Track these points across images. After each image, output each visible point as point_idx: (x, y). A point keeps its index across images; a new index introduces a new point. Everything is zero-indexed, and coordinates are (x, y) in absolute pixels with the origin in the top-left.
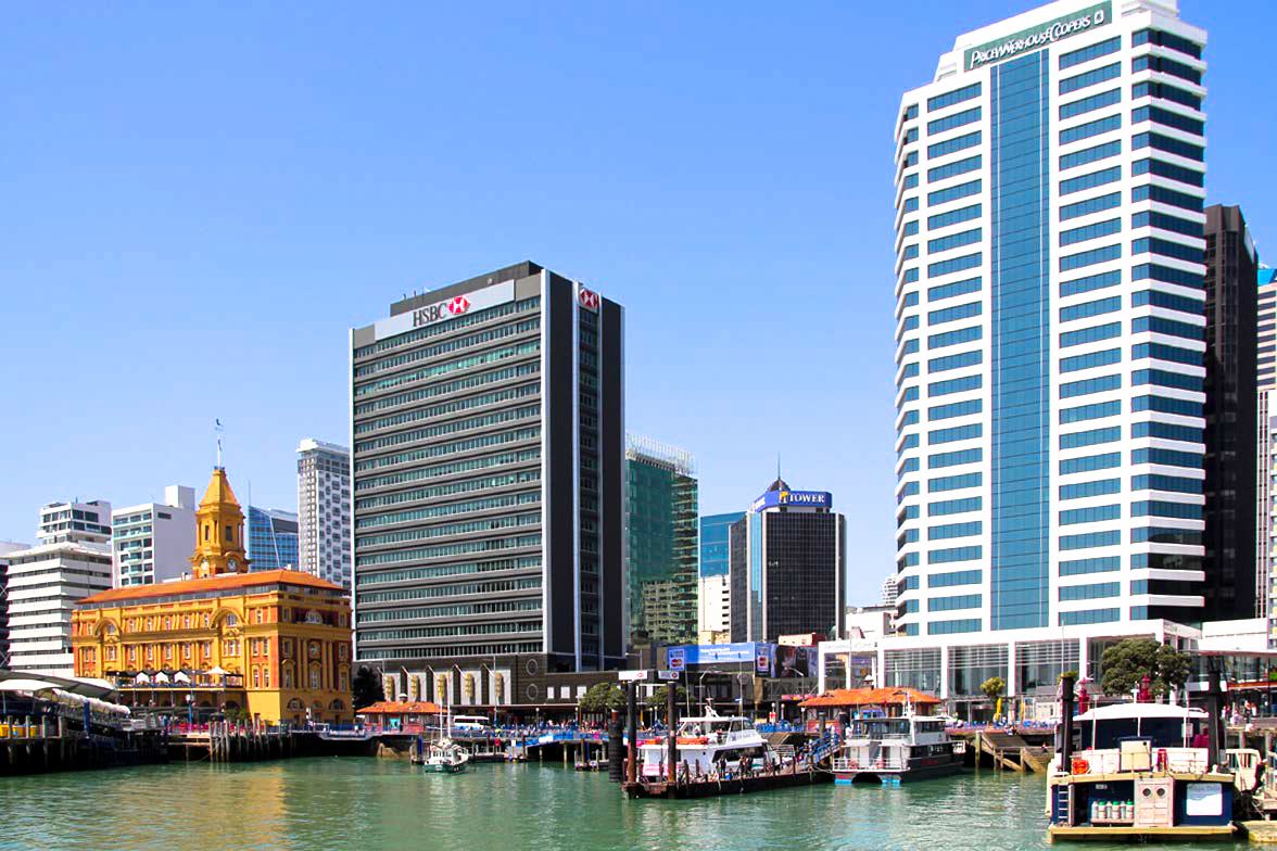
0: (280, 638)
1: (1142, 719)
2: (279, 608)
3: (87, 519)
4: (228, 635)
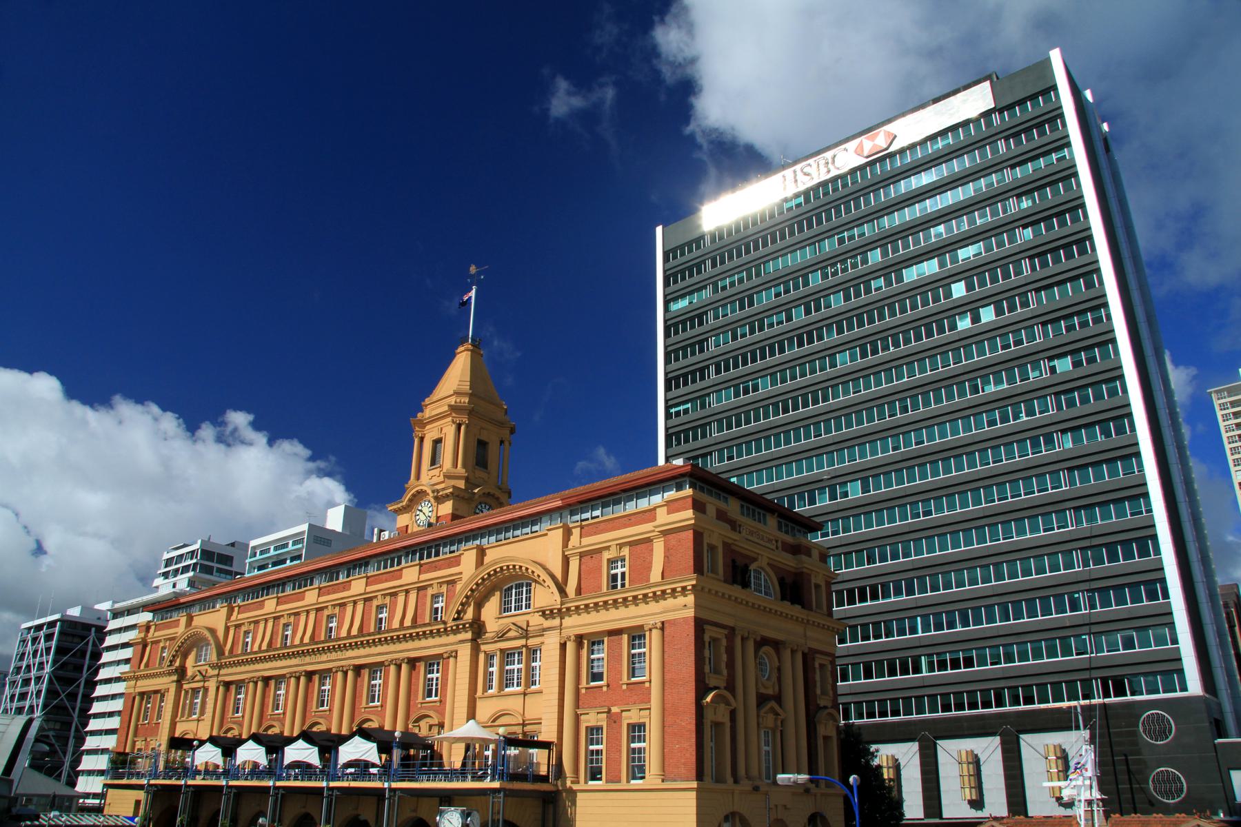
0: (700, 624)
1: (1179, 648)
2: (698, 537)
3: (218, 562)
4: (502, 636)
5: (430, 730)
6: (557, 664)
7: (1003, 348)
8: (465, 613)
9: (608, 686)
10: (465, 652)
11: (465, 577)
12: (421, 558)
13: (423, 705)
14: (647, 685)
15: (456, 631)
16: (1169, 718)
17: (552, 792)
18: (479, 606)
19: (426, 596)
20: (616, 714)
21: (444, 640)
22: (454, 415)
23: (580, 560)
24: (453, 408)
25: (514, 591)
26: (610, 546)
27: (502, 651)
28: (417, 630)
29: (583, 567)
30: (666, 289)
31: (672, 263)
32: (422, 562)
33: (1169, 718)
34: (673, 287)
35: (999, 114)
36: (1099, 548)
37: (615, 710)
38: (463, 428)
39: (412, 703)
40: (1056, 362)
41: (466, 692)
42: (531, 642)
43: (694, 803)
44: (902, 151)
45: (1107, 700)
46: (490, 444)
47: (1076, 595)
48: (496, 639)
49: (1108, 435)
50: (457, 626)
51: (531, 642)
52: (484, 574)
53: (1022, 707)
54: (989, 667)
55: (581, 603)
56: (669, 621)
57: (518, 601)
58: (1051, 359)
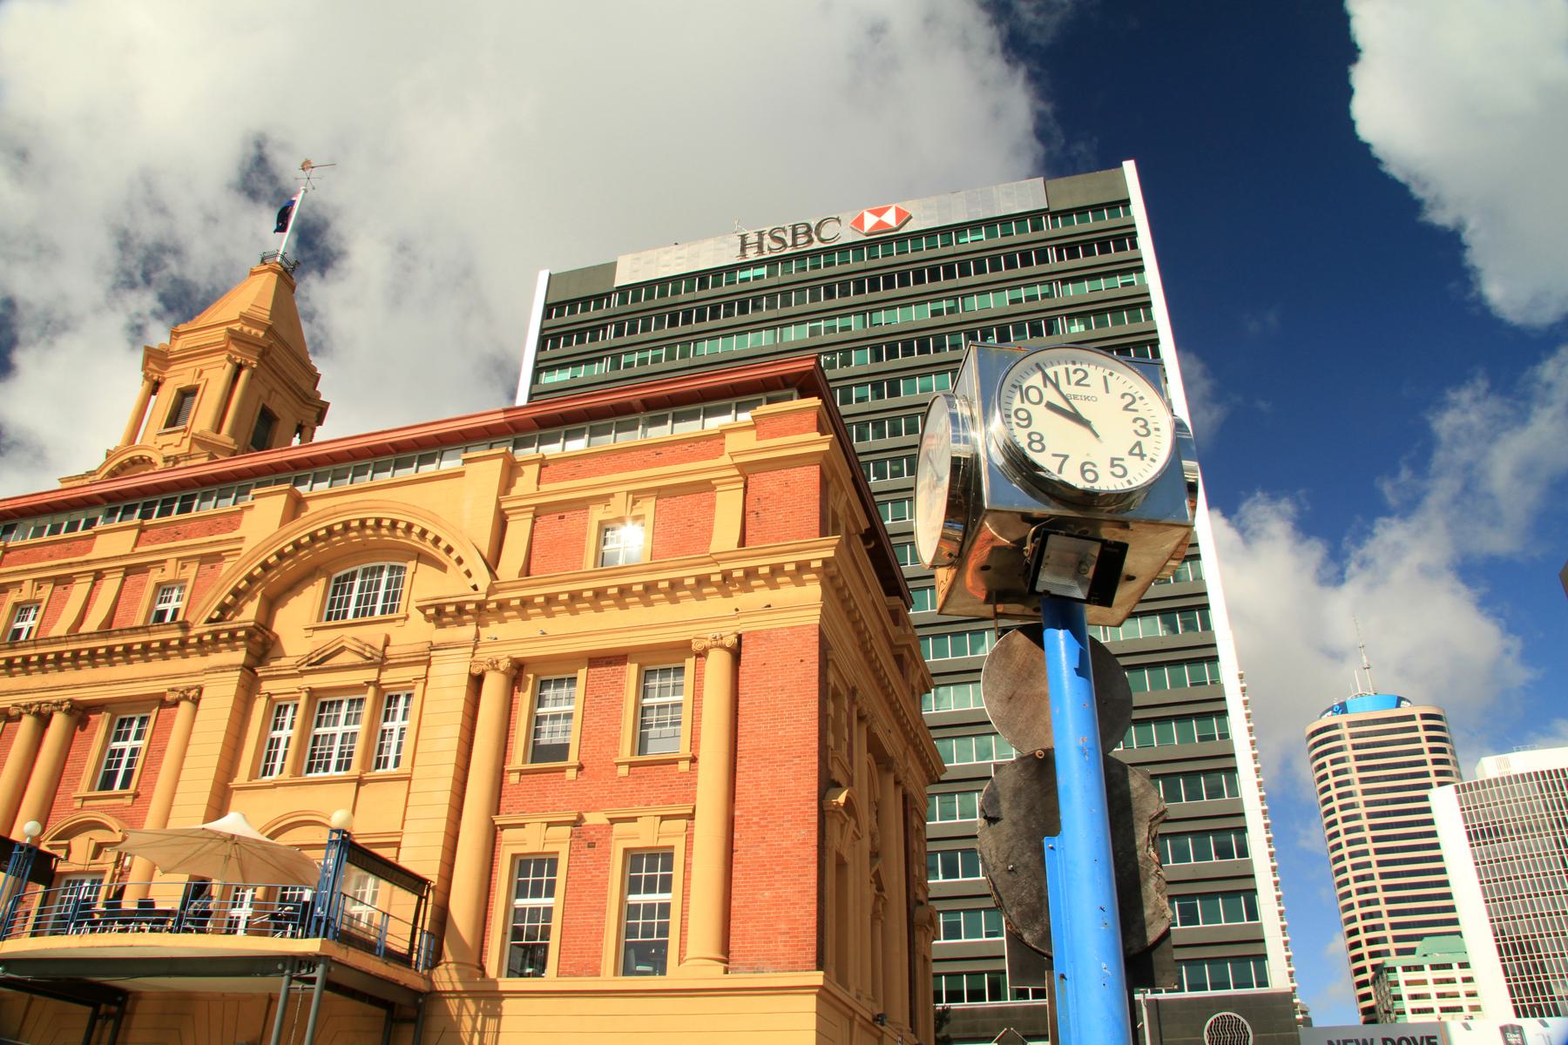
4: (319, 662)
5: (96, 855)
6: (458, 718)
8: (239, 612)
9: (580, 768)
10: (221, 694)
11: (246, 547)
12: (146, 515)
13: (87, 803)
14: (684, 766)
15: (203, 647)
16: (1245, 1022)
17: (417, 993)
18: (272, 604)
19: (142, 585)
20: (597, 827)
21: (176, 665)
22: (233, 348)
23: (534, 522)
24: (235, 337)
25: (357, 582)
26: (612, 495)
27: (312, 693)
28: (111, 642)
29: (538, 535)
30: (540, 353)
31: (554, 321)
32: (147, 522)
33: (1245, 1022)
34: (549, 352)
37: (594, 818)
38: (244, 374)
39: (59, 798)
41: (211, 773)
42: (389, 676)
43: (810, 1021)
44: (916, 236)
46: (281, 422)
48: (304, 667)
49: (1174, 629)
50: (215, 635)
51: (389, 676)
52: (303, 535)
54: (984, 939)
55: (538, 593)
56: (754, 635)
57: (366, 603)
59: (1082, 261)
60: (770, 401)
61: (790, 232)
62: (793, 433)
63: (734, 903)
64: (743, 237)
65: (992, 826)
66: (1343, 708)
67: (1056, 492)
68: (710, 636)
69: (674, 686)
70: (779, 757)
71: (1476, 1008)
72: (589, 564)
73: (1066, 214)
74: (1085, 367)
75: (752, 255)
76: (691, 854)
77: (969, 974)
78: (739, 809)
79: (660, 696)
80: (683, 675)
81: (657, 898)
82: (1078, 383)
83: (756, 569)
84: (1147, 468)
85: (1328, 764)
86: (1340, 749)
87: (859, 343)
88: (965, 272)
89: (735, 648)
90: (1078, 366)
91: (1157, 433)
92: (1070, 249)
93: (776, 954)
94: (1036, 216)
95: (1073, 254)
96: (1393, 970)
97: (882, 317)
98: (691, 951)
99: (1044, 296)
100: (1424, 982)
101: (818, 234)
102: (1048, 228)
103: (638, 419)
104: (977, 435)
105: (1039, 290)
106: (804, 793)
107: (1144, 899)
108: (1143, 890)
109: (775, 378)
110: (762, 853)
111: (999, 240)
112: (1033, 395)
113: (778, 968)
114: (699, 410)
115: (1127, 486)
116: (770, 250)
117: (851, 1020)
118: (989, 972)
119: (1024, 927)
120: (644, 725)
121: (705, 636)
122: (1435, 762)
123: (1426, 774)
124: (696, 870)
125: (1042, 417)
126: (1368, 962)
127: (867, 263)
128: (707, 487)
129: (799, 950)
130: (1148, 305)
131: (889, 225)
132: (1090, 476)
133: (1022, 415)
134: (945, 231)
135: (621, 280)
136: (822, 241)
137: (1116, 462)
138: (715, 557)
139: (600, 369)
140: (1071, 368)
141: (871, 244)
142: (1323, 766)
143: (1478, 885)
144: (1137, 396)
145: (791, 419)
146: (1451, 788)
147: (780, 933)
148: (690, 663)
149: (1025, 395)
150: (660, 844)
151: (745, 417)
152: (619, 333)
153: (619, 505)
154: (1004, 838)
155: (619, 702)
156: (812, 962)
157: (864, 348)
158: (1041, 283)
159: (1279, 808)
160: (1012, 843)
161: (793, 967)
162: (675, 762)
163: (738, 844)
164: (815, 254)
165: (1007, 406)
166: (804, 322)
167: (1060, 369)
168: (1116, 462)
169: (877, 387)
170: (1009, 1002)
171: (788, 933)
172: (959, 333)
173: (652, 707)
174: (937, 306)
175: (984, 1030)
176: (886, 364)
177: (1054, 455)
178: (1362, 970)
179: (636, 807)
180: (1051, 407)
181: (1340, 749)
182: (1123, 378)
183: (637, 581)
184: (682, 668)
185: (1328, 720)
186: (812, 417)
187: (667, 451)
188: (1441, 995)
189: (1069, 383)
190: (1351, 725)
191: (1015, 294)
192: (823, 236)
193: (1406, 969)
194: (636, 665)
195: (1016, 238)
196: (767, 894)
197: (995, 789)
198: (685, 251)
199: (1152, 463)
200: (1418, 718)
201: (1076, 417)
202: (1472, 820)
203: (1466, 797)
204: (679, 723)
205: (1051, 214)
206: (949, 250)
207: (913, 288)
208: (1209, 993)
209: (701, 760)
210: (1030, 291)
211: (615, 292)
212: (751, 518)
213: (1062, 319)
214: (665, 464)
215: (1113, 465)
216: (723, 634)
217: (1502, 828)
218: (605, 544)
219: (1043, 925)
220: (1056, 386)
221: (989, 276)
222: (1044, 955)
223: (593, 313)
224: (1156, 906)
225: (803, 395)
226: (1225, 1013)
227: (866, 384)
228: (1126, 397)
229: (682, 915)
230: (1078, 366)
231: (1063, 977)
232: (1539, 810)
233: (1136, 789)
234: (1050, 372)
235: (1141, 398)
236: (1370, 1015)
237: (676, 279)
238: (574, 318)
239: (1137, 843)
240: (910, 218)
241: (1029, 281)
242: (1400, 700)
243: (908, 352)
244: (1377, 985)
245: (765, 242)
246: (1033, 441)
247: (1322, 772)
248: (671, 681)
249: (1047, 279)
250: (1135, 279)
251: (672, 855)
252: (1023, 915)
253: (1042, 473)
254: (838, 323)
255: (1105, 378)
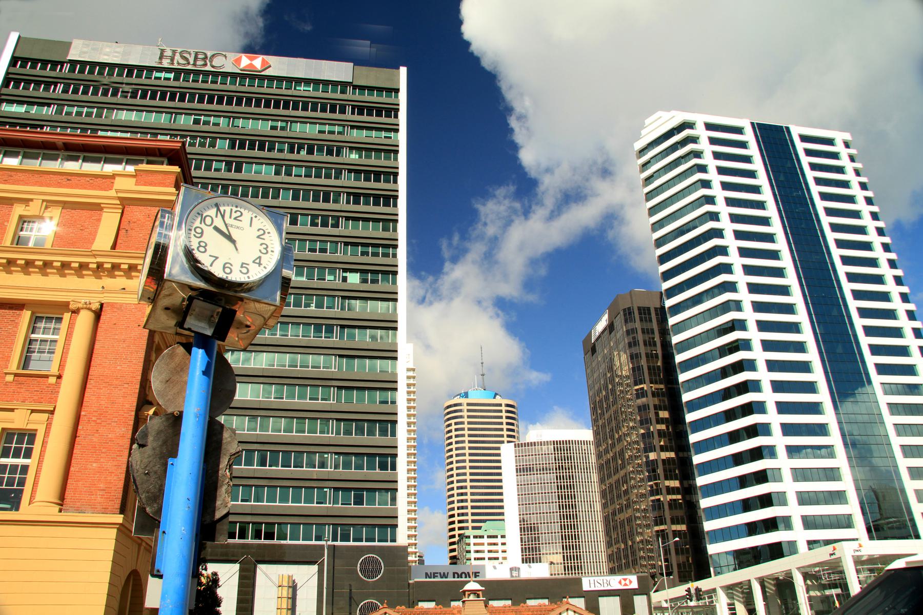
7: (310, 250)
14: (52, 380)
16: (381, 561)
26: (32, 200)
33: (381, 561)
35: (353, 89)
36: (350, 423)
40: (348, 274)
43: (111, 545)
44: (271, 78)
45: (335, 543)
47: (326, 456)
53: (263, 541)
54: (240, 503)
56: (112, 305)
58: (345, 270)
59: (365, 118)
60: (149, 163)
61: (193, 56)
62: (159, 186)
63: (72, 469)
64: (162, 51)
65: (141, 449)
66: (466, 395)
67: (207, 276)
68: (83, 301)
69: (54, 329)
70: (115, 382)
71: (505, 558)
72: (8, 241)
73: (362, 88)
74: (242, 210)
75: (166, 63)
76: (48, 435)
77: (266, 523)
78: (84, 411)
79: (43, 334)
80: (61, 323)
81: (21, 461)
82: (235, 219)
83: (119, 265)
84: (261, 271)
85: (453, 424)
86: (461, 417)
87: (223, 135)
88: (296, 108)
89: (98, 311)
90: (239, 209)
91: (272, 253)
92: (360, 109)
93: (95, 503)
94: (344, 85)
95: (361, 113)
96: (468, 537)
97: (240, 122)
98: (38, 497)
99: (339, 133)
100: (483, 544)
101: (211, 62)
102: (350, 95)
103: (59, 154)
104: (173, 234)
105: (337, 129)
106: (127, 406)
107: (218, 496)
108: (218, 491)
109: (155, 148)
110: (95, 440)
111: (320, 94)
112: (208, 221)
113: (95, 510)
114: (102, 158)
115: (247, 280)
116: (178, 64)
117: (140, 545)
118: (240, 522)
119: (147, 504)
120: (29, 351)
121: (79, 301)
122: (508, 430)
123: (502, 436)
124: (50, 446)
125: (210, 234)
126: (457, 532)
127: (237, 87)
128: (98, 208)
129: (110, 501)
130: (396, 152)
131: (256, 68)
132: (228, 270)
133: (199, 230)
134: (290, 80)
135: (73, 55)
136: (213, 67)
137: (244, 265)
138: (94, 253)
139: (47, 111)
140: (234, 209)
141: (243, 76)
142: (449, 425)
143: (517, 496)
144: (266, 231)
145: (160, 177)
146: (513, 444)
147: (99, 490)
148: (67, 316)
149: (203, 220)
150: (28, 428)
151: (131, 169)
152: (65, 91)
153: (33, 209)
154: (146, 456)
155: (14, 334)
156: (117, 509)
157: (226, 139)
158: (339, 125)
159: (419, 445)
160: (151, 459)
161: (105, 511)
162: (47, 377)
163: (80, 432)
164: (207, 74)
165: (191, 224)
166: (191, 114)
167: (228, 209)
168: (244, 265)
169: (229, 164)
170: (249, 541)
171: (104, 490)
172: (285, 143)
173: (37, 340)
174: (275, 124)
175: (233, 556)
176: (237, 152)
177: (210, 256)
178: (453, 536)
179: (15, 402)
180: (217, 229)
181: (461, 417)
182: (262, 220)
183: (39, 259)
184: (62, 318)
185: (457, 400)
186: (172, 179)
187: (75, 180)
188: (490, 551)
189: (230, 217)
190: (468, 404)
191: (323, 128)
192: (214, 64)
193: (475, 537)
194: (30, 312)
195: (330, 95)
196: (94, 465)
197: (147, 429)
198: (120, 48)
199: (264, 269)
200: (503, 405)
201: (229, 237)
202: (520, 462)
203: (519, 450)
204: (53, 353)
205: (353, 86)
206: (289, 92)
207: (262, 110)
208: (364, 543)
209: (64, 377)
210: (332, 128)
211: (67, 63)
212: (122, 232)
213: (346, 148)
214: (72, 187)
215: (242, 267)
216: (91, 301)
217: (533, 467)
218: (22, 230)
219: (158, 504)
220: (223, 217)
221: (309, 113)
222: (156, 520)
223: (48, 72)
224: (224, 500)
225: (171, 163)
226: (371, 555)
227: (222, 161)
228: (261, 231)
229: (36, 474)
230: (239, 209)
231: (164, 532)
232: (552, 460)
233: (226, 438)
234: (222, 209)
235: (269, 233)
236: (454, 560)
237: (112, 66)
238: (33, 72)
239: (220, 467)
240: (270, 67)
241: (332, 122)
242: (496, 394)
243: (252, 147)
244: (459, 544)
245: (176, 58)
246: (200, 246)
247: (449, 429)
248: (52, 325)
249: (343, 123)
250: (392, 136)
251: (35, 435)
252: (148, 498)
253: (199, 265)
254: (212, 119)
255: (252, 218)
